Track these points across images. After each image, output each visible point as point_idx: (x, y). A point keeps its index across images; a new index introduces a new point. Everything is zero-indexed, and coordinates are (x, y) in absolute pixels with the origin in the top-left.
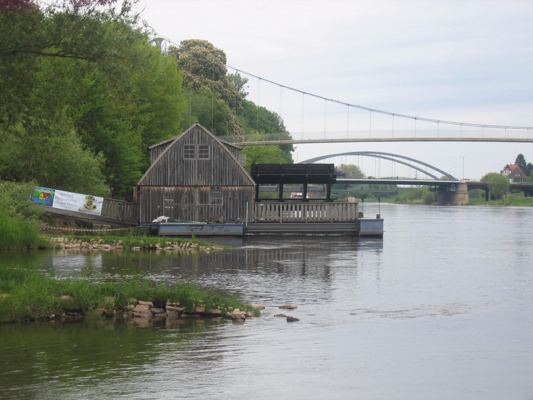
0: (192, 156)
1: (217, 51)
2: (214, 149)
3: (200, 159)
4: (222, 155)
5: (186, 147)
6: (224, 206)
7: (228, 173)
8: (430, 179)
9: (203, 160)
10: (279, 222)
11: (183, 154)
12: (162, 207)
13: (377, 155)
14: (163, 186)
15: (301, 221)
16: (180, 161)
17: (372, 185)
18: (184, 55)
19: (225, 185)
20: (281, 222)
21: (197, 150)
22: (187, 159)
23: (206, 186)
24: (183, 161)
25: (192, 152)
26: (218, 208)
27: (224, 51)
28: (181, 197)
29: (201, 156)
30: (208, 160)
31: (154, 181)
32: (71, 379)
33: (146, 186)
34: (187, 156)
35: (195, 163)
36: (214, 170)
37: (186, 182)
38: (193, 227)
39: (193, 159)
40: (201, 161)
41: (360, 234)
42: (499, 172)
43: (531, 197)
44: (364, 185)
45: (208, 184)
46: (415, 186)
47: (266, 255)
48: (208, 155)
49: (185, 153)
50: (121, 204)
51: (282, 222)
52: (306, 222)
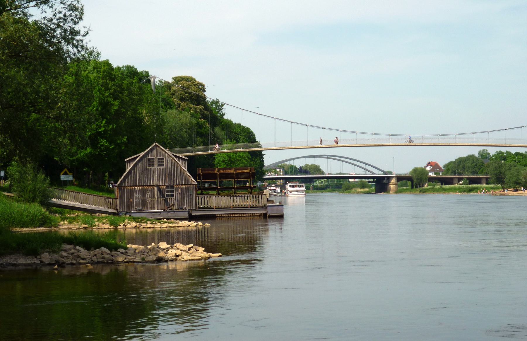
0: (153, 166)
1: (198, 83)
2: (168, 160)
3: (159, 167)
4: (173, 164)
5: (149, 159)
6: (175, 199)
7: (178, 176)
8: (369, 174)
9: (161, 168)
10: (213, 208)
11: (147, 164)
12: (133, 200)
13: (332, 157)
14: (133, 186)
15: (228, 207)
16: (145, 168)
17: (330, 179)
18: (175, 88)
19: (176, 184)
20: (215, 208)
21: (156, 161)
22: (150, 167)
23: (163, 185)
24: (147, 169)
25: (153, 162)
26: (171, 200)
27: (203, 83)
28: (146, 193)
29: (159, 165)
30: (164, 168)
31: (127, 183)
32: (143, 322)
33: (129, 186)
34: (149, 165)
35: (155, 170)
36: (168, 175)
37: (149, 183)
38: (154, 213)
39: (154, 167)
40: (159, 168)
41: (268, 215)
42: (423, 167)
43: (445, 186)
44: (323, 180)
45: (184, 183)
46: (357, 180)
47: (248, 231)
48: (164, 164)
49: (148, 163)
50: (106, 199)
51: (216, 208)
52: (232, 208)
